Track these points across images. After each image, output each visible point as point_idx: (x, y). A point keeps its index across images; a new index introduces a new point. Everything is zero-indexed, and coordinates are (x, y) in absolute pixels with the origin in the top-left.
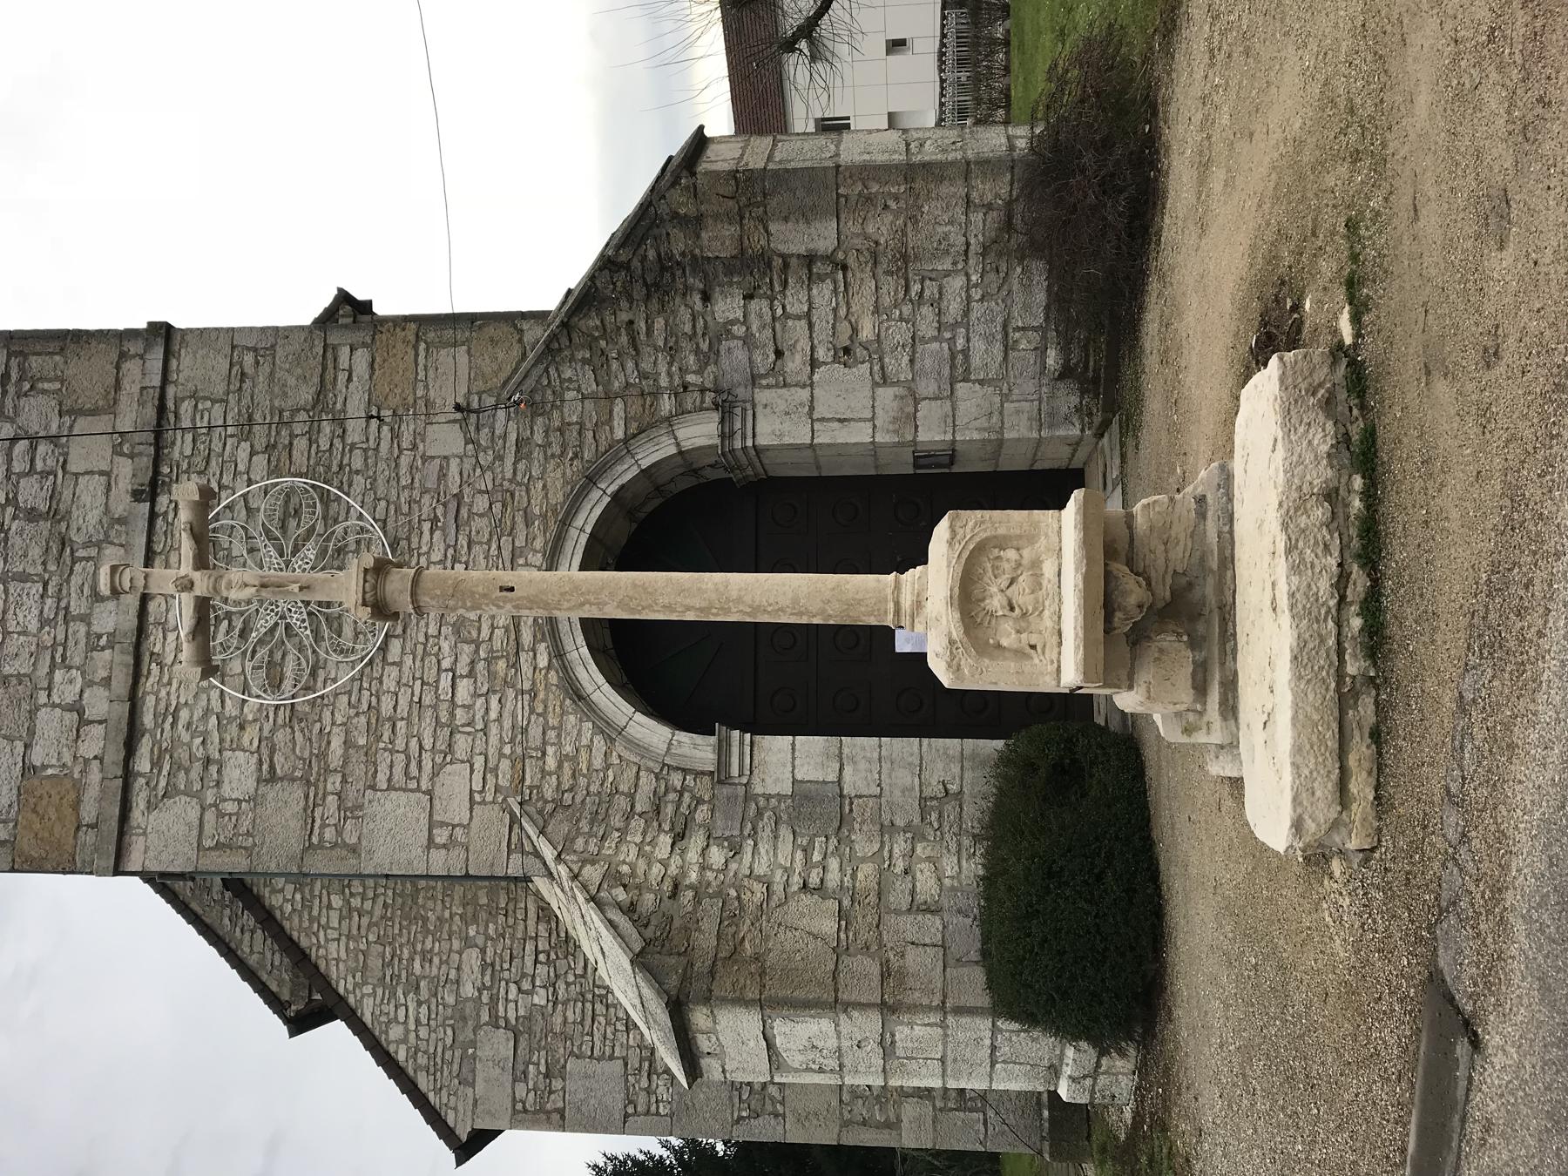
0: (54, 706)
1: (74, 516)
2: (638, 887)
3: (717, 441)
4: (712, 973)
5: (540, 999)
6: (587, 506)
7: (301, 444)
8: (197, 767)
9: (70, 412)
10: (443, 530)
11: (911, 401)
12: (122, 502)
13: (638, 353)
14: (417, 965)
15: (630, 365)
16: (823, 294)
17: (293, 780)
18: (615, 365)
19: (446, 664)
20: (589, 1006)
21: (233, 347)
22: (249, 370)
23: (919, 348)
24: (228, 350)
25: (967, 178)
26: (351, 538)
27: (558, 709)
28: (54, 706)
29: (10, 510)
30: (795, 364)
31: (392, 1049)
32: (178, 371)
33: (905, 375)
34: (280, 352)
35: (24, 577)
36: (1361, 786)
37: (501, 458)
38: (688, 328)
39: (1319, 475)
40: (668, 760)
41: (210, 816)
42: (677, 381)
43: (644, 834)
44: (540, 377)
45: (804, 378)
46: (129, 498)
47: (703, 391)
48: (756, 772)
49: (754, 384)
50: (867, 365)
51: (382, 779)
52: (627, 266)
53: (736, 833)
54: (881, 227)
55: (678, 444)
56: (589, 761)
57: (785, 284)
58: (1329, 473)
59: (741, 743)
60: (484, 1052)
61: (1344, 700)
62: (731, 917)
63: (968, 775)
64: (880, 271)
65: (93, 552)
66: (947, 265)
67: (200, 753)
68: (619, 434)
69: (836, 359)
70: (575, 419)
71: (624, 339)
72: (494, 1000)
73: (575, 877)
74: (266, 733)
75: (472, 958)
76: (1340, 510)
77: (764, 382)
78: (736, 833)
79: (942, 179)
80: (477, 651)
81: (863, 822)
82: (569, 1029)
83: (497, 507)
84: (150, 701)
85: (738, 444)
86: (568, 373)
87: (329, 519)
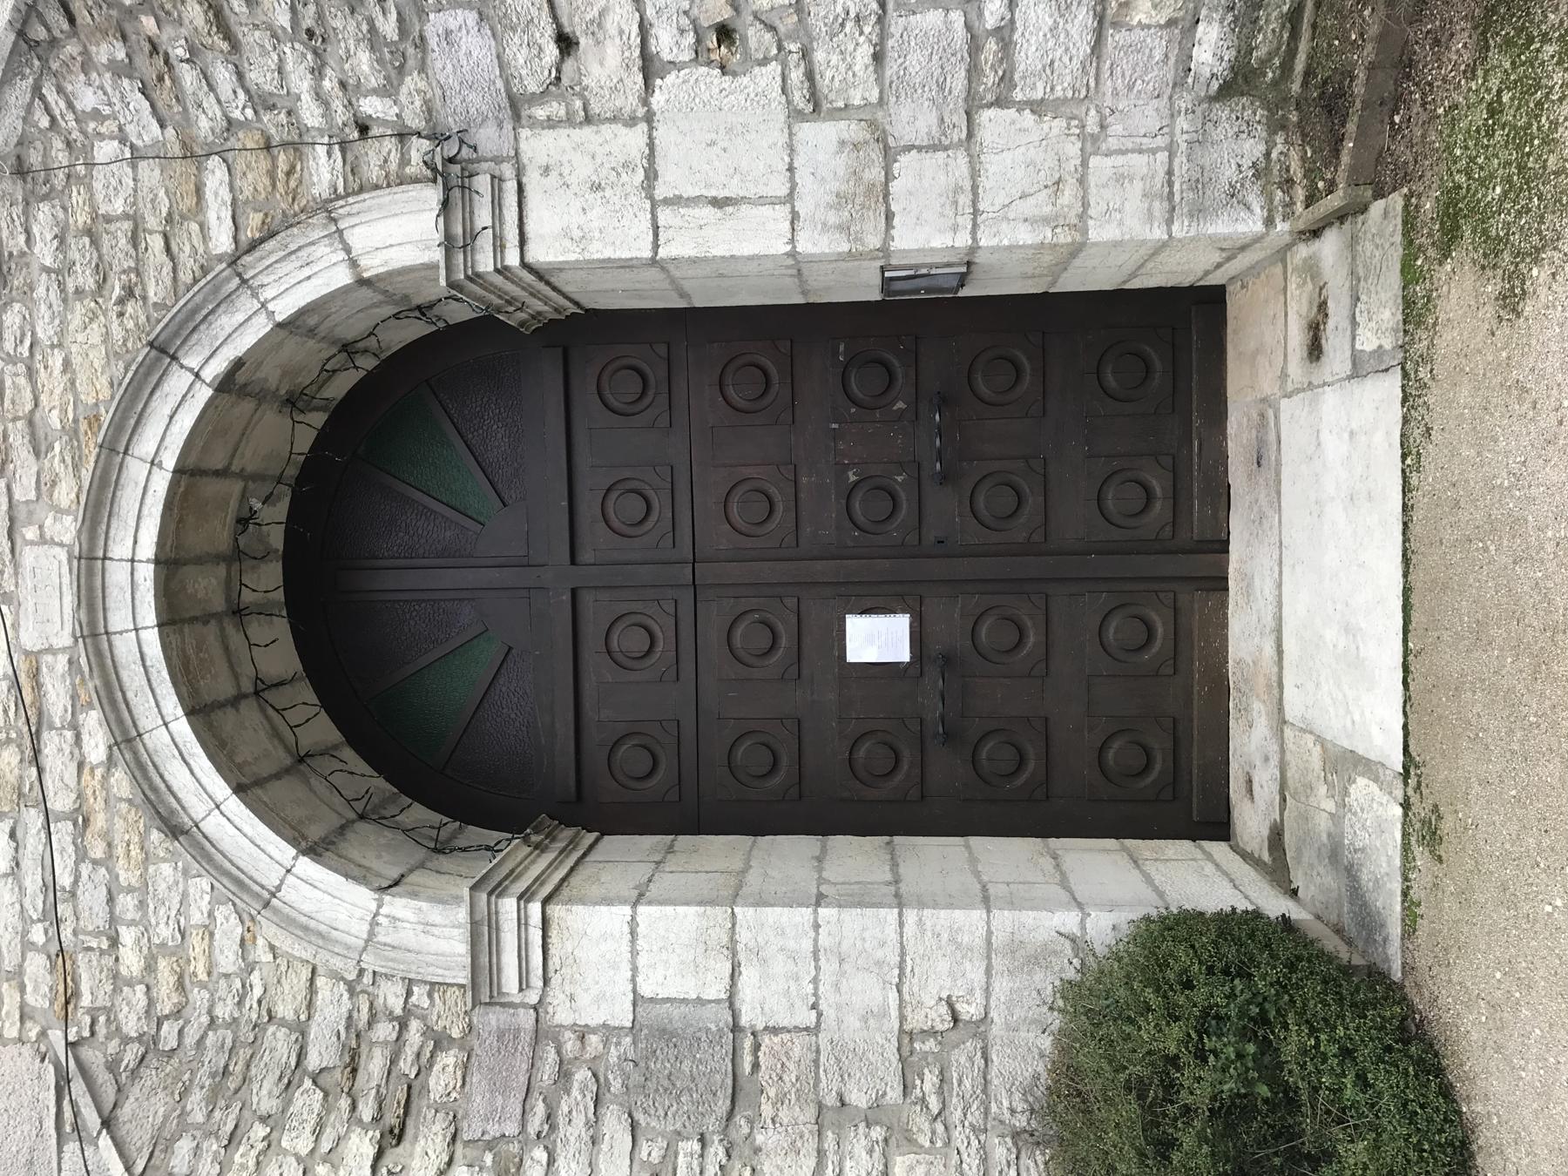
3: (438, 255)
6: (161, 408)
11: (876, 154)
13: (235, 46)
15: (223, 76)
18: (188, 77)
27: (135, 851)
30: (606, 66)
33: (864, 91)
40: (370, 962)
42: (341, 115)
43: (318, 1133)
44: (29, 109)
45: (630, 101)
47: (402, 136)
48: (555, 981)
50: (774, 68)
53: (511, 1128)
55: (354, 264)
56: (209, 954)
59: (523, 923)
63: (1001, 986)
68: (222, 241)
69: (700, 55)
70: (118, 206)
77: (540, 113)
78: (511, 1128)
81: (781, 1099)
85: (485, 262)
86: (88, 99)
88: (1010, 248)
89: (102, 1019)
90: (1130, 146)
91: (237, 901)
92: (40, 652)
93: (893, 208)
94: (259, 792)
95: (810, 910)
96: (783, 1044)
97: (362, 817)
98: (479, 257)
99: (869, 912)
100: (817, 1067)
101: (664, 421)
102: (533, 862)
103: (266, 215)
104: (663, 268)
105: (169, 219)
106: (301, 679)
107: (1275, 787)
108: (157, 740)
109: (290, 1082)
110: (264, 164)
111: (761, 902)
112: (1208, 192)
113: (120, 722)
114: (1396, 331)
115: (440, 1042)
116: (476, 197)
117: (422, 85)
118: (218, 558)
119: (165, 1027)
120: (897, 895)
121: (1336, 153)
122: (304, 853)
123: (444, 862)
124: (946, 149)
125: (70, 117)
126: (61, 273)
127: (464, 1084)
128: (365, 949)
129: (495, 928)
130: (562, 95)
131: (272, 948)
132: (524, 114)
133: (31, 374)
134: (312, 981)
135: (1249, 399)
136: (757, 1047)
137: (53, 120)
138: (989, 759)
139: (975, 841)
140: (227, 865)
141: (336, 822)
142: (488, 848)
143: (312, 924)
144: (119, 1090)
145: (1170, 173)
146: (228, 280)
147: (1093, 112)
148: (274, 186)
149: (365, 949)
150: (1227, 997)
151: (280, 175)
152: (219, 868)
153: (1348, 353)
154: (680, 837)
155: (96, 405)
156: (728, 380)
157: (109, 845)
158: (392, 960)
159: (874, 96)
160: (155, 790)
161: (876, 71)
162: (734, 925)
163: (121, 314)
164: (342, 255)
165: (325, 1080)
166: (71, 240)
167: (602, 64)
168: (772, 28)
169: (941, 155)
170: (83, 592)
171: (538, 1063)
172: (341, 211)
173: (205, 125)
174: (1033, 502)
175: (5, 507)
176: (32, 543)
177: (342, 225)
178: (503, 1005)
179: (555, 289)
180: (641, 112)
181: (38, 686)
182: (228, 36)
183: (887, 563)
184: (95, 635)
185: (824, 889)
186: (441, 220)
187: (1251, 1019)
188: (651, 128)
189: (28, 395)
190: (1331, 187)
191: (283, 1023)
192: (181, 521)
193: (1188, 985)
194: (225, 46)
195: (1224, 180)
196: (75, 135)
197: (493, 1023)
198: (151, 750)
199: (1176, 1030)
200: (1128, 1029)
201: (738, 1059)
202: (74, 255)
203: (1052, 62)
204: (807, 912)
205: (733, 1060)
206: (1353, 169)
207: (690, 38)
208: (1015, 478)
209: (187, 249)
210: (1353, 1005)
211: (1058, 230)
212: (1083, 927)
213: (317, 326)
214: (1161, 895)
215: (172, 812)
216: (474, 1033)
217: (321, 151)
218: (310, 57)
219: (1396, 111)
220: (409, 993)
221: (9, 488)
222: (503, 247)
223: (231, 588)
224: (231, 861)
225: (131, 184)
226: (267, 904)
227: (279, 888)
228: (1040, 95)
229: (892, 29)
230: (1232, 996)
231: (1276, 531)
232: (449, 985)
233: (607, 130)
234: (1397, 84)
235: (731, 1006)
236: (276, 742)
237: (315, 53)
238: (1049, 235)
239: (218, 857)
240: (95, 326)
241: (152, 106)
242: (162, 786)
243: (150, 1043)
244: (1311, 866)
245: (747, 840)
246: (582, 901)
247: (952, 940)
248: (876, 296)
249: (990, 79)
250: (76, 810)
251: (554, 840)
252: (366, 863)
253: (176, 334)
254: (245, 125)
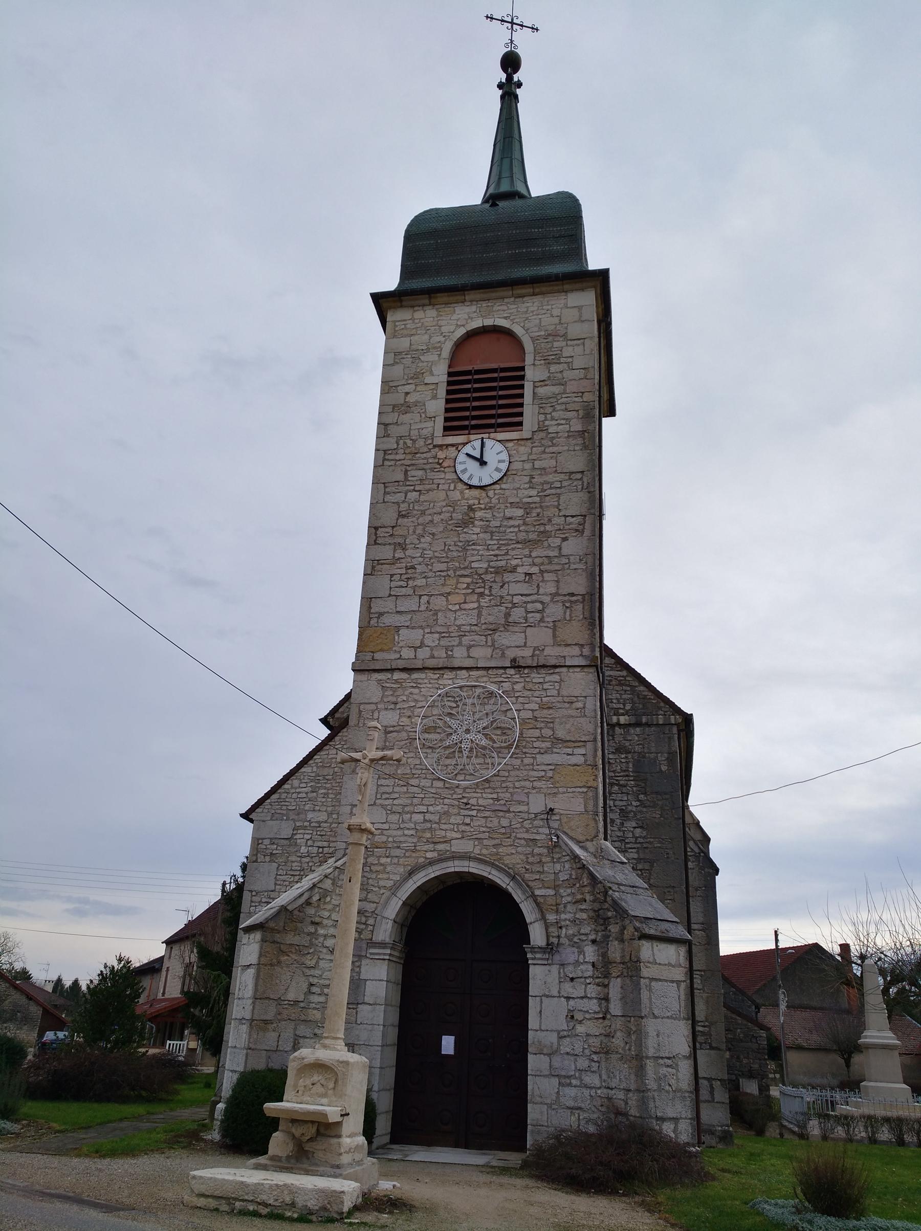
0: (424, 636)
1: (507, 634)
2: (318, 906)
4: (274, 942)
5: (303, 849)
6: (502, 876)
7: (537, 733)
8: (394, 699)
9: (554, 626)
10: (493, 804)
11: (549, 1052)
12: (511, 654)
14: (323, 791)
15: (569, 899)
16: (593, 1005)
17: (385, 742)
18: (569, 891)
19: (431, 809)
20: (298, 873)
21: (585, 697)
22: (574, 705)
23: (572, 1058)
24: (584, 694)
25: (638, 1091)
26: (489, 761)
28: (424, 636)
29: (510, 605)
30: (568, 988)
31: (289, 782)
32: (574, 672)
33: (564, 1050)
34: (582, 720)
35: (479, 615)
36: (202, 1202)
37: (527, 831)
38: (582, 931)
39: (300, 1202)
40: (379, 918)
41: (373, 707)
42: (563, 923)
45: (563, 993)
46: (512, 656)
51: (382, 782)
52: (605, 901)
54: (618, 1041)
57: (598, 985)
58: (300, 1205)
59: (385, 954)
60: (284, 824)
61: (228, 1200)
62: (299, 950)
64: (603, 1038)
65: (490, 643)
66: (604, 1077)
67: (399, 700)
68: (537, 892)
71: (579, 897)
72: (305, 828)
73: (326, 876)
74: (406, 728)
75: (323, 817)
76: (287, 1207)
79: (637, 1076)
80: (436, 823)
82: (289, 864)
83: (503, 830)
84: (423, 676)
87: (499, 750)
108: (430, 870)
129: (384, 948)
133: (511, 845)
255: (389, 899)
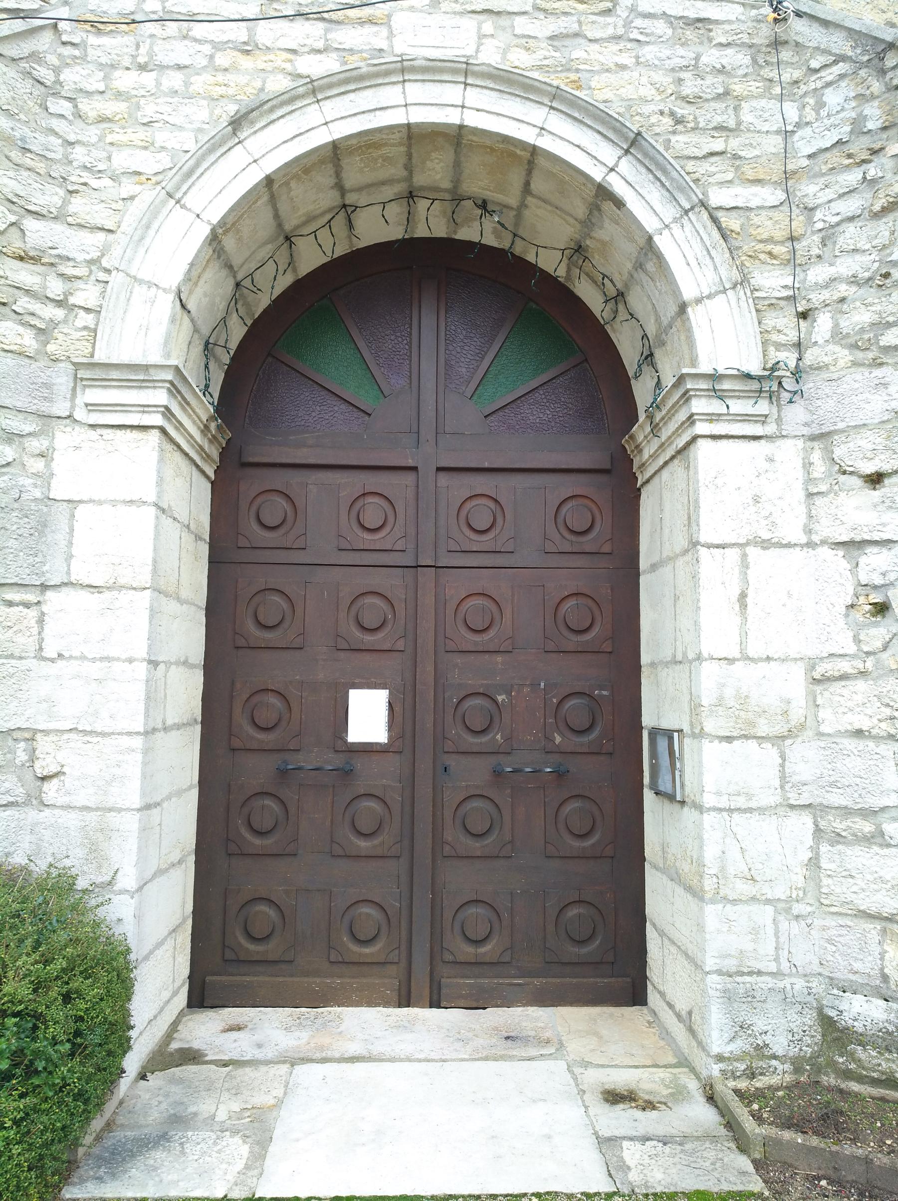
3: (705, 367)
6: (587, 138)
11: (780, 729)
13: (876, 216)
15: (851, 206)
18: (853, 177)
27: (221, 90)
30: (857, 511)
40: (116, 279)
42: (816, 298)
48: (93, 434)
49: (813, 438)
50: (852, 649)
55: (699, 301)
56: (130, 145)
59: (145, 408)
63: (72, 820)
68: (718, 197)
70: (747, 117)
77: (816, 456)
85: (699, 406)
86: (833, 98)
88: (700, 838)
89: (77, 53)
90: (782, 940)
91: (174, 171)
92: (390, 27)
93: (735, 742)
94: (265, 198)
95: (145, 656)
96: (28, 628)
97: (238, 285)
98: (703, 401)
99: (142, 707)
100: (7, 657)
101: (550, 547)
102: (194, 422)
103: (738, 234)
104: (686, 551)
105: (736, 157)
106: (351, 245)
107: (235, 1056)
108: (312, 115)
109: (13, 203)
110: (779, 235)
111: (154, 613)
112: (744, 1006)
113: (330, 86)
114: (646, 1185)
115: (44, 333)
116: (753, 401)
117: (841, 363)
118: (457, 182)
119: (68, 105)
120: (154, 730)
121: (788, 1124)
122: (213, 231)
123: (198, 348)
124: (782, 787)
125: (819, 84)
126: (695, 67)
127: (6, 351)
128: (128, 275)
130: (831, 476)
131: (132, 198)
132: (816, 444)
133: (617, 38)
134: (102, 229)
135: (560, 1029)
136: (27, 605)
137: (816, 71)
138: (263, 807)
139: (195, 793)
140: (205, 165)
141: (236, 262)
142: (207, 386)
143: (151, 232)
144: (14, 60)
145: (759, 973)
146: (689, 199)
147: (809, 909)
148: (761, 241)
149: (128, 275)
150: (54, 1038)
151: (769, 247)
152: (203, 158)
153: (617, 1133)
154: (207, 547)
155: (590, 88)
156: (582, 600)
157: (226, 70)
158: (118, 298)
159: (824, 729)
160: (272, 110)
161: (846, 731)
162: (134, 589)
163: (662, 113)
164: (706, 293)
165: (14, 233)
166: (721, 78)
167: (857, 508)
168: (885, 648)
169: (777, 783)
170: (439, 64)
171: (21, 416)
172: (742, 292)
173: (809, 190)
174: (476, 846)
175: (510, 9)
176: (479, 28)
177: (730, 293)
178: (74, 389)
179: (666, 463)
180: (816, 538)
181: (362, 22)
182: (885, 211)
183: (430, 725)
184: (403, 71)
185: (162, 667)
186: (735, 372)
187: (32, 1062)
188: (802, 546)
189: (598, 34)
190: (758, 1118)
191: (65, 203)
192: (492, 150)
193: (67, 998)
194: (877, 208)
195: (755, 1019)
196: (804, 88)
197: (58, 380)
198: (304, 109)
199: (24, 991)
200: (29, 942)
201: (16, 589)
202: (710, 80)
203: (851, 876)
204: (142, 651)
205: (16, 584)
206: (778, 1142)
207: (879, 581)
208: (496, 833)
209: (713, 169)
210: (41, 1157)
211: (715, 880)
212: (121, 892)
213: (645, 271)
214: (146, 958)
215: (252, 123)
216: (51, 364)
217: (789, 281)
218: (867, 275)
219: (831, 1182)
220: (88, 310)
221: (524, 13)
222: (711, 421)
223: (432, 193)
224: (208, 168)
225: (765, 129)
226: (170, 195)
227: (183, 207)
228: (824, 864)
229: (883, 746)
230: (55, 1042)
231: (454, 1055)
232: (94, 344)
233: (803, 509)
234: (853, 1183)
235: (65, 584)
236: (303, 219)
237: (870, 279)
238: (712, 872)
239: (212, 158)
240: (654, 92)
241: (827, 149)
242: (274, 116)
243: (54, 90)
244: (167, 1096)
245: (203, 603)
246: (161, 460)
247: (114, 778)
248: (648, 720)
249: (840, 825)
250: (257, 45)
251: (210, 441)
252: (202, 282)
253: (646, 155)
254: (810, 221)
255: (154, 212)
